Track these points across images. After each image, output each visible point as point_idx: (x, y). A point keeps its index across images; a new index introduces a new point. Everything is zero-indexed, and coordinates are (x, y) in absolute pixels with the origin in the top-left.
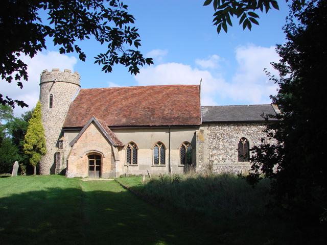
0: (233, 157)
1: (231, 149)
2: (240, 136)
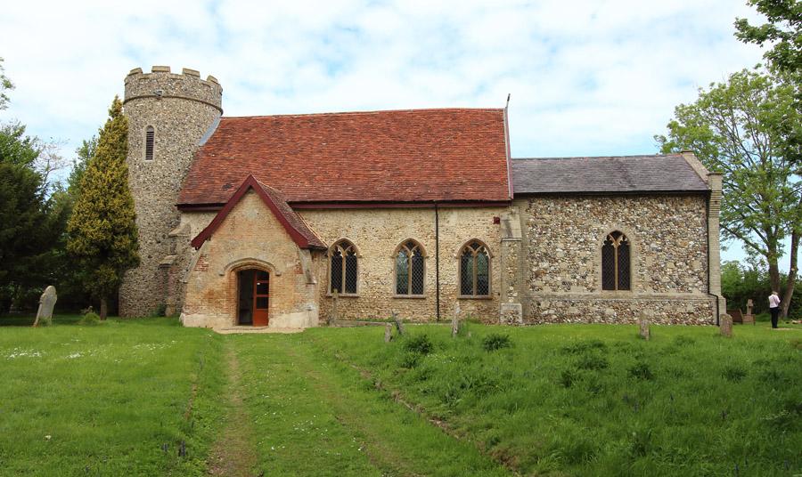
1: (585, 260)
2: (607, 228)
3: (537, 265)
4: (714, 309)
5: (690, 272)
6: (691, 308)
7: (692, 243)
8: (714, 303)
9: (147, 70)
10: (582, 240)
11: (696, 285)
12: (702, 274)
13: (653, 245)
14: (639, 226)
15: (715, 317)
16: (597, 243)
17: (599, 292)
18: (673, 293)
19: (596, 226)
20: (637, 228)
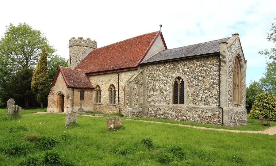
0: (167, 99)
1: (166, 90)
2: (175, 76)
3: (149, 93)
4: (221, 115)
5: (211, 95)
6: (209, 114)
7: (212, 81)
8: (221, 112)
9: (92, 40)
10: (165, 81)
11: (214, 102)
12: (217, 97)
13: (194, 83)
14: (188, 74)
15: (221, 119)
16: (171, 82)
17: (171, 105)
18: (202, 106)
19: (171, 75)
20: (187, 75)
